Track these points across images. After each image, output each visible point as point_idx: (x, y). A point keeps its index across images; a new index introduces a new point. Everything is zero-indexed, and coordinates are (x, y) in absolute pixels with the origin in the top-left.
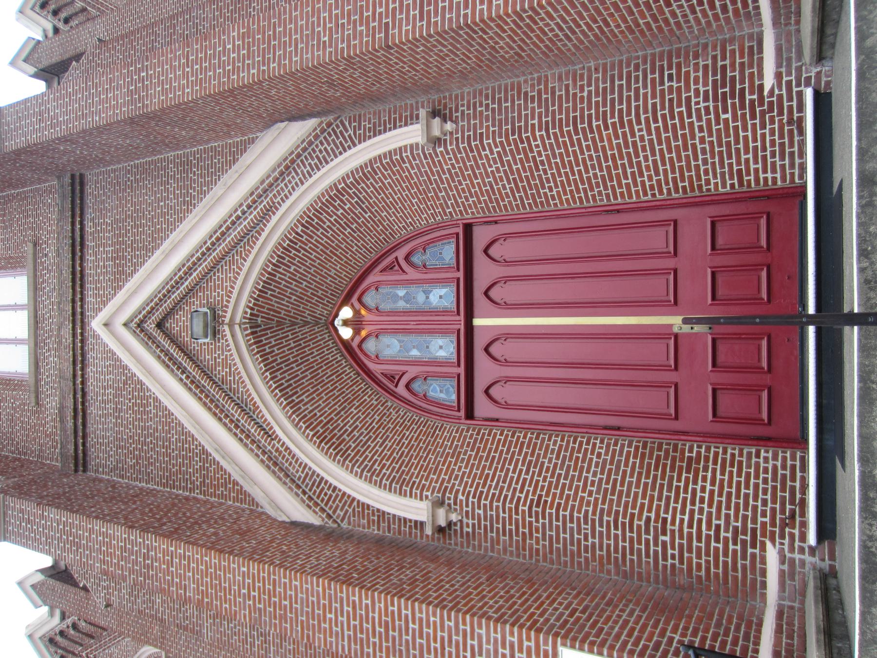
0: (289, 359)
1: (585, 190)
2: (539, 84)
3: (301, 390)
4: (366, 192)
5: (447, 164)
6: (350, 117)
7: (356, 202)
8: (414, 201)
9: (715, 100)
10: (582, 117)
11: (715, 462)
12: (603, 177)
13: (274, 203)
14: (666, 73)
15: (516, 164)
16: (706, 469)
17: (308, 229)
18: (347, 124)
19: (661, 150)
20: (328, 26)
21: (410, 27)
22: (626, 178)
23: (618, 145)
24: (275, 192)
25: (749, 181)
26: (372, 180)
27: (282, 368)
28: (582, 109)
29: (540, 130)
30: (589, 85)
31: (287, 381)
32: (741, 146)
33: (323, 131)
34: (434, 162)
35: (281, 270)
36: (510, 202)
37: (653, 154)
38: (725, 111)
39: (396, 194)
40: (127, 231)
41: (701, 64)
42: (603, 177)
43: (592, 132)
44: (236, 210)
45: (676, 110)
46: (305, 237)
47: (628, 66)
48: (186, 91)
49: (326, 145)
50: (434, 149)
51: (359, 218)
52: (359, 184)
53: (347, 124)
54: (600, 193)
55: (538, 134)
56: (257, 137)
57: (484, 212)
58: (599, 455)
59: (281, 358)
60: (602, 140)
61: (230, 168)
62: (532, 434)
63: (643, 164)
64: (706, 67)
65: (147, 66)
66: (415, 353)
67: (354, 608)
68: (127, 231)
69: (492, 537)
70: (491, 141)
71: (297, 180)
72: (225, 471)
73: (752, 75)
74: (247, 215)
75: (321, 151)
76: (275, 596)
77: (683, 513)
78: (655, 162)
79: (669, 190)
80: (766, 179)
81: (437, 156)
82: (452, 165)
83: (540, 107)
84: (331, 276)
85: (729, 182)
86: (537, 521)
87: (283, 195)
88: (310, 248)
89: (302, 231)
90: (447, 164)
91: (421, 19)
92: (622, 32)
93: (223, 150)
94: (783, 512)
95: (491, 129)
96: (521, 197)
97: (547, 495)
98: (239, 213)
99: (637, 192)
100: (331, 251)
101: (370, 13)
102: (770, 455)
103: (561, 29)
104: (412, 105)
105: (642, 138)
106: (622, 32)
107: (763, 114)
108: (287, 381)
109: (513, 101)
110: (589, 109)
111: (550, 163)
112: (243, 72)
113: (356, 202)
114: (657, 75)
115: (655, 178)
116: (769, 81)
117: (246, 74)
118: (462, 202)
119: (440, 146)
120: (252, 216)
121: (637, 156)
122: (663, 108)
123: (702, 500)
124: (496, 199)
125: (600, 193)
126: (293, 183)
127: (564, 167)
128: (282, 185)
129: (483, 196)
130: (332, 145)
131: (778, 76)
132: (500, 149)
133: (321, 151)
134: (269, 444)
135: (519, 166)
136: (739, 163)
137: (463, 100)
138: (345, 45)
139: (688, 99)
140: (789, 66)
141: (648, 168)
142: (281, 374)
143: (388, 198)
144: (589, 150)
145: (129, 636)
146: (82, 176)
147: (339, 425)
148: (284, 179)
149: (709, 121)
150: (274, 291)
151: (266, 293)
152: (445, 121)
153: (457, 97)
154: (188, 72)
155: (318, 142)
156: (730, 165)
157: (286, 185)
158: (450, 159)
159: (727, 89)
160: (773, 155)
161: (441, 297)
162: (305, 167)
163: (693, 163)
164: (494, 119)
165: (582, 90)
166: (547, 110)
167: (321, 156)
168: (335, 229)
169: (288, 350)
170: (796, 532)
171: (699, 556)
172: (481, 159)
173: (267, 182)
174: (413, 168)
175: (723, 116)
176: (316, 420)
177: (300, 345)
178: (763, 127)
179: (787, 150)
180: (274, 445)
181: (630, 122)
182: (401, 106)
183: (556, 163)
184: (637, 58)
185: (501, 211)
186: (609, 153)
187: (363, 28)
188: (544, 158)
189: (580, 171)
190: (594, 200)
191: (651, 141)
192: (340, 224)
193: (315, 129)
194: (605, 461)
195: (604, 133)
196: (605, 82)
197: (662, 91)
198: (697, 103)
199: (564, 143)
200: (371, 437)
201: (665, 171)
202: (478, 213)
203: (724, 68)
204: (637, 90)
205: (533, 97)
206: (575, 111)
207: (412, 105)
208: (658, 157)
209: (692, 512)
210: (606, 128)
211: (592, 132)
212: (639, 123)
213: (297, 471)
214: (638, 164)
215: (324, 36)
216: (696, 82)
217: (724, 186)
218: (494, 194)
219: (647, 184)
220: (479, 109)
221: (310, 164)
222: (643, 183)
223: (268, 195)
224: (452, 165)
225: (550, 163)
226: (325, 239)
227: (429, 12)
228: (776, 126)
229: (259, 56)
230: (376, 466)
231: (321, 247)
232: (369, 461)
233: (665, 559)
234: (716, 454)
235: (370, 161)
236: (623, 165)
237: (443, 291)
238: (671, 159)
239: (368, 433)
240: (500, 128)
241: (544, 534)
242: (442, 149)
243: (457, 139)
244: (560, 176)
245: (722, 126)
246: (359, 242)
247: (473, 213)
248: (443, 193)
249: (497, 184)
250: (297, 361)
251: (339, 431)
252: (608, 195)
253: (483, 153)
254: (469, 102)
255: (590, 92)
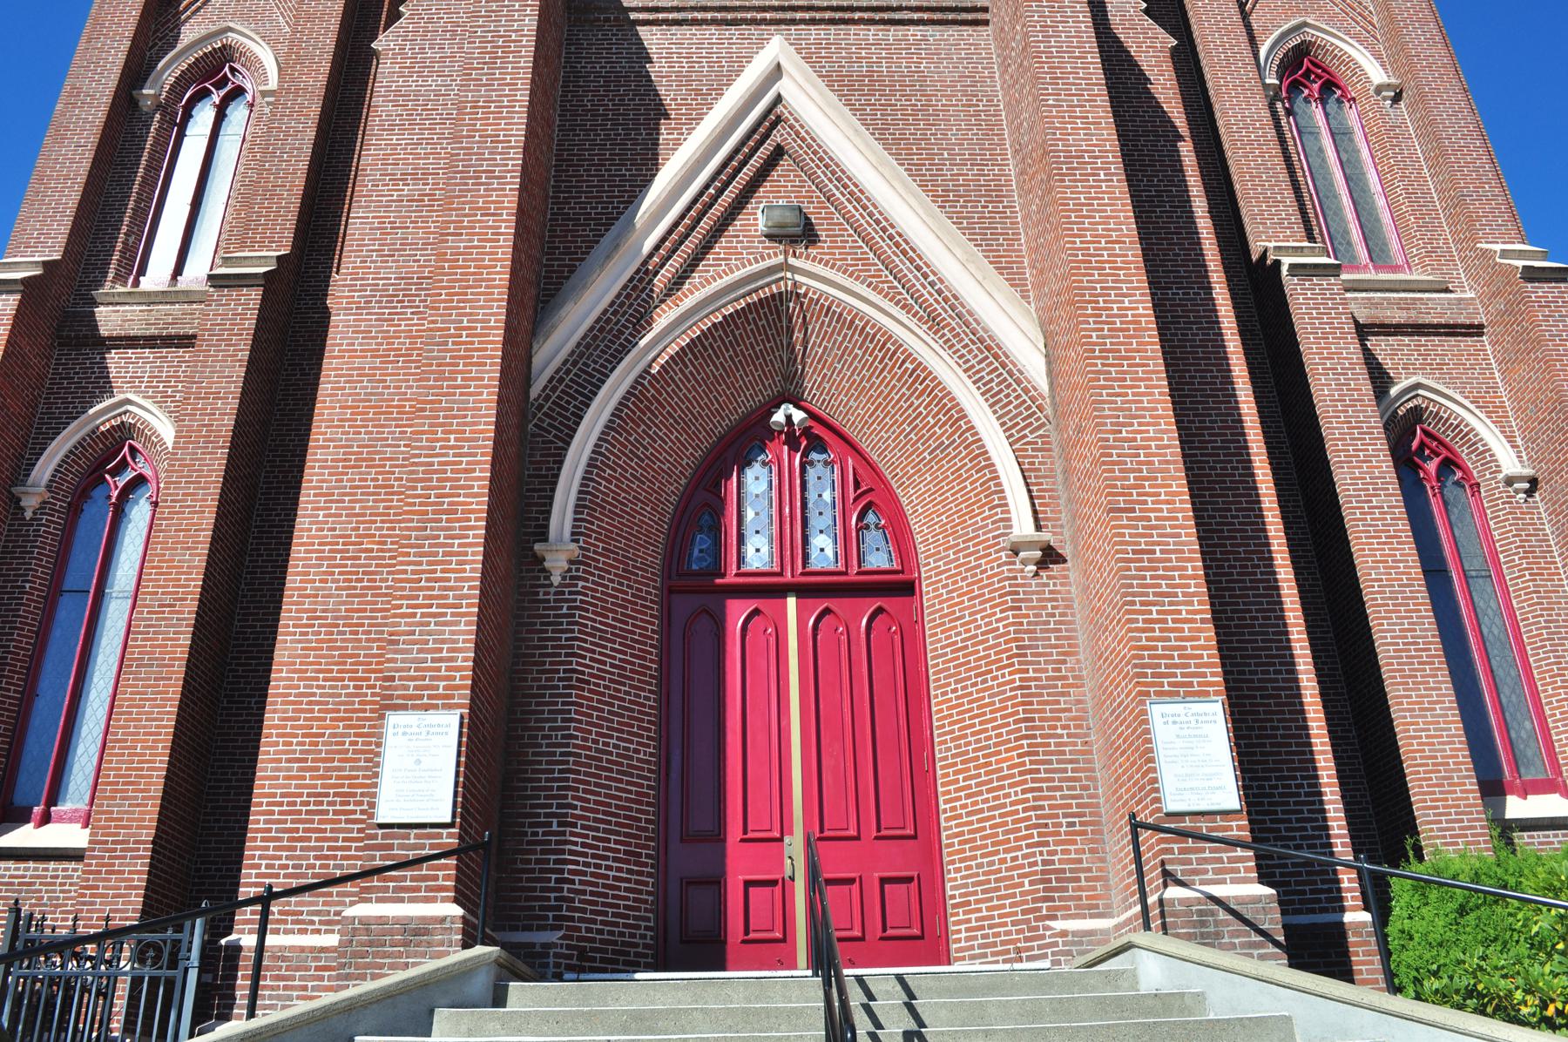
0: (739, 345)
1: (952, 732)
2: (1074, 677)
3: (700, 364)
4: (955, 457)
5: (986, 564)
6: (1048, 436)
7: (943, 443)
8: (943, 517)
9: (1044, 873)
10: (1033, 728)
11: (637, 882)
12: (967, 752)
13: (943, 328)
14: (1076, 820)
15: (984, 650)
16: (630, 871)
17: (910, 376)
18: (1041, 432)
19: (993, 817)
20: (1139, 436)
21: (1127, 538)
22: (965, 779)
23: (1001, 770)
24: (958, 330)
25: (957, 914)
26: (969, 465)
27: (727, 336)
28: (1042, 728)
29: (1021, 679)
30: (1069, 736)
31: (711, 344)
32: (995, 902)
33: (1033, 399)
34: (989, 547)
35: (856, 337)
36: (940, 641)
37: (990, 809)
38: (1031, 883)
39: (952, 495)
40: (908, 97)
41: (1084, 857)
42: (967, 752)
43: (1017, 739)
44: (935, 274)
45: (1035, 832)
46: (900, 372)
47: (1087, 778)
48: (1078, 240)
49: (1015, 403)
50: (1003, 549)
51: (923, 444)
52: (965, 448)
53: (1041, 432)
54: (949, 749)
55: (1017, 676)
56: (1029, 303)
57: (928, 607)
58: (637, 751)
59: (741, 334)
60: (1007, 751)
61: (991, 263)
62: (656, 670)
63: (979, 798)
64: (1080, 861)
65: (1112, 180)
66: (750, 514)
67: (466, 471)
68: (908, 97)
69: (536, 624)
70: (1011, 620)
71: (973, 362)
72: (588, 253)
73: (1068, 908)
74: (929, 288)
75: (1007, 396)
76: (465, 365)
77: (584, 845)
78: (981, 811)
79: (950, 828)
80: (959, 931)
81: (996, 552)
82: (986, 571)
83: (1048, 678)
84: (849, 400)
85: (957, 893)
86: (560, 679)
87: (954, 341)
88: (885, 377)
89: (907, 369)
90: (986, 564)
91: (1134, 552)
92: (1116, 770)
93: (1014, 251)
94: (593, 950)
95: (1025, 621)
96: (946, 654)
97: (590, 691)
98: (932, 278)
99: (949, 792)
100: (880, 404)
101: (1147, 490)
102: (648, 941)
103: (1119, 706)
104: (1059, 519)
105: (1007, 796)
106: (1116, 770)
107: (1027, 921)
108: (711, 344)
109: (1056, 646)
110: (1042, 736)
111: (984, 690)
112: (1095, 322)
113: (943, 443)
114: (1075, 810)
115: (964, 811)
116: (1058, 925)
117: (1092, 326)
118: (941, 580)
119: (1007, 556)
120: (927, 296)
121: (989, 791)
122: (1038, 817)
123: (598, 866)
124: (943, 624)
125: (949, 749)
126: (969, 357)
127: (979, 708)
128: (967, 341)
129: (948, 607)
130: (1015, 412)
131: (1064, 934)
132: (1002, 631)
133: (1007, 396)
134: (627, 320)
135: (982, 654)
136: (977, 902)
137: (1062, 584)
138: (1115, 458)
139: (1047, 844)
140: (1073, 943)
141: (976, 803)
142: (720, 336)
143: (947, 484)
144: (997, 736)
145: (294, 32)
146: (986, 23)
147: (657, 418)
148: (974, 343)
149: (1022, 866)
150: (829, 326)
151: (826, 315)
152: (1036, 564)
153: (1066, 577)
154: (1100, 242)
155: (1020, 391)
156: (975, 893)
157: (966, 346)
158: (992, 568)
159: (1054, 884)
160: (985, 937)
161: (822, 550)
162: (988, 374)
163: (979, 853)
164: (1037, 623)
165: (1064, 727)
166: (1043, 687)
167: (1001, 396)
168: (910, 411)
169: (751, 343)
170: (574, 962)
171: (538, 861)
172: (992, 607)
173: (971, 320)
174: (983, 520)
175: (1026, 881)
176: (662, 387)
177: (758, 359)
178: (1014, 923)
179: (988, 950)
180: (627, 328)
181: (1025, 781)
182: (1058, 505)
183: (984, 698)
184: (1096, 788)
185: (930, 629)
186: (993, 759)
187: (1132, 481)
188: (990, 683)
189: (973, 725)
190: (941, 743)
191: (1004, 806)
192: (915, 419)
193: (1036, 390)
194: (631, 758)
195: (1015, 753)
196: (1071, 752)
197: (1057, 816)
198: (1041, 853)
199: (1006, 708)
200: (643, 461)
201: (971, 823)
202: (928, 600)
203: (1078, 880)
204: (1060, 789)
205: (1059, 670)
206: (1041, 720)
207: (1059, 519)
208: (986, 814)
209: (585, 855)
210: (1019, 756)
211: (1017, 739)
212: (1024, 792)
213: (595, 362)
214: (981, 793)
215: (1127, 432)
216: (1064, 852)
217: (953, 888)
218: (950, 621)
219: (958, 804)
220: (1049, 605)
221: (992, 380)
222: (959, 798)
223: (953, 319)
224: (986, 571)
225: (984, 690)
226: (897, 398)
227: (1141, 560)
228: (1014, 937)
229: (1111, 344)
230: (608, 471)
231: (886, 392)
232: (614, 462)
233: (532, 825)
234: (646, 884)
235: (993, 465)
236: (979, 775)
237: (829, 552)
238: (984, 829)
239: (647, 457)
240: (1026, 632)
241: (545, 687)
242: (1004, 559)
243: (1015, 578)
244: (970, 702)
245: (1017, 881)
246: (893, 441)
247: (928, 593)
248: (952, 557)
249: (962, 625)
250: (737, 356)
251: (649, 418)
252: (945, 758)
253: (998, 610)
254: (1059, 592)
255: (1061, 736)
